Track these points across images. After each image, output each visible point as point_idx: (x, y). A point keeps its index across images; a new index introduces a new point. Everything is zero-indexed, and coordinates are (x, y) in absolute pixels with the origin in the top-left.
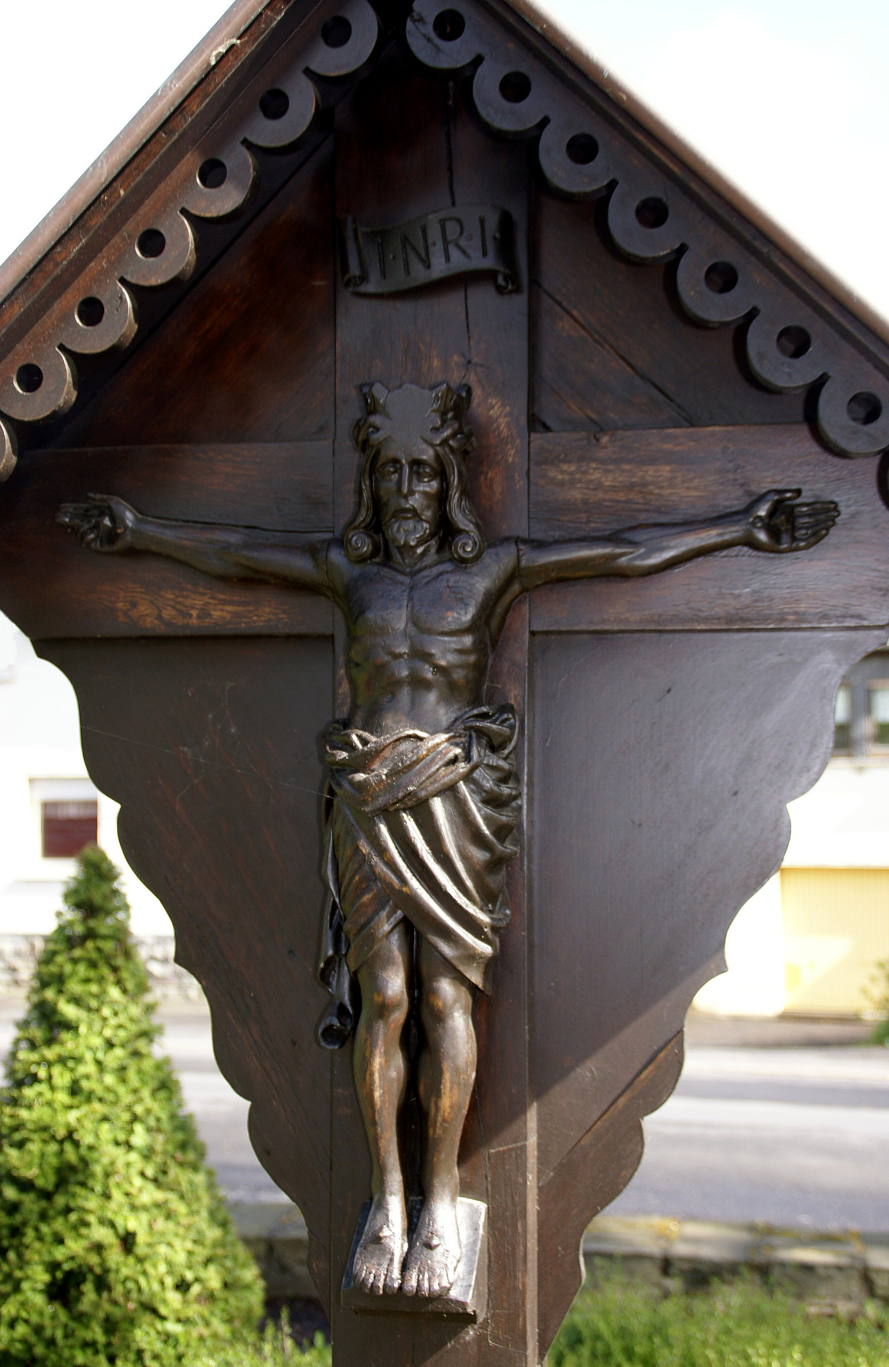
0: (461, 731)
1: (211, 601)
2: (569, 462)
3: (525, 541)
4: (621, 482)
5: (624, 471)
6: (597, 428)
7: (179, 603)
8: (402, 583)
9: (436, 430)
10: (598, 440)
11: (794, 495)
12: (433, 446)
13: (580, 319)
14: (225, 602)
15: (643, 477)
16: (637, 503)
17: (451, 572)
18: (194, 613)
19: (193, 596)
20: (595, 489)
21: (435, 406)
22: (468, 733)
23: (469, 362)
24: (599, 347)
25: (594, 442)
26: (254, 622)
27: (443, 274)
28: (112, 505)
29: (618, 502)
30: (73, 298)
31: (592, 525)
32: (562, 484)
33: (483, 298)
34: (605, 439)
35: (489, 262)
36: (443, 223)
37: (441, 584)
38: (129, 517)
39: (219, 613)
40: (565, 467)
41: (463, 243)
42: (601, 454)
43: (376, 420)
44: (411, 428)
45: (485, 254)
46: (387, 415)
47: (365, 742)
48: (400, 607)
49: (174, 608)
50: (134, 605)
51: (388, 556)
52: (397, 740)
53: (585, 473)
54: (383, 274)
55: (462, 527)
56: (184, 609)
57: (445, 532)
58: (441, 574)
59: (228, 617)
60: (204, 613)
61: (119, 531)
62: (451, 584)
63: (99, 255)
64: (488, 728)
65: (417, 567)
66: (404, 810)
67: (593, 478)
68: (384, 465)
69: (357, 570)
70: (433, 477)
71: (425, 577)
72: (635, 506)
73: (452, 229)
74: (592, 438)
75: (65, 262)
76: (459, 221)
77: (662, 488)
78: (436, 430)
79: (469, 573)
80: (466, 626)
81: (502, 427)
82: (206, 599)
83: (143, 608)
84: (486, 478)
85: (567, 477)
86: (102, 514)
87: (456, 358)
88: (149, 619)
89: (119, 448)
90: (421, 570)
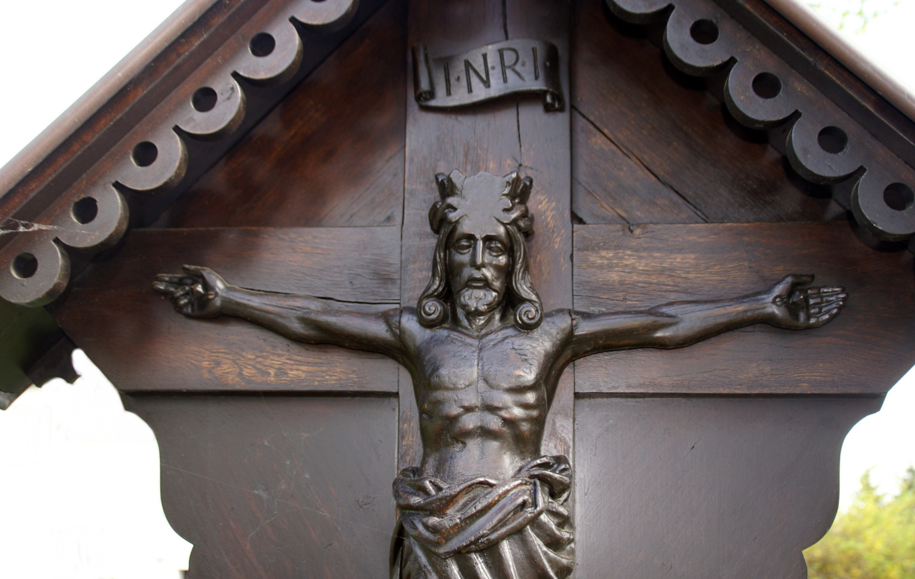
0: (527, 479)
1: (288, 362)
2: (607, 249)
3: (577, 313)
4: (652, 267)
5: (655, 258)
6: (629, 225)
7: (259, 362)
8: (471, 345)
9: (507, 210)
10: (632, 231)
11: (809, 279)
12: (504, 225)
13: (610, 136)
14: (300, 363)
15: (671, 263)
16: (667, 285)
17: (515, 336)
18: (272, 372)
19: (272, 357)
20: (630, 273)
21: (506, 192)
22: (532, 481)
23: (520, 165)
24: (626, 158)
25: (629, 233)
26: (327, 380)
27: (502, 93)
28: (205, 274)
29: (651, 283)
30: (190, 86)
31: (629, 302)
32: (601, 267)
33: (532, 115)
34: (638, 231)
35: (538, 85)
36: (501, 52)
37: (507, 346)
38: (220, 285)
39: (295, 372)
40: (603, 253)
41: (518, 68)
42: (634, 243)
43: (451, 200)
44: (481, 211)
45: (536, 78)
46: (462, 197)
47: (439, 489)
48: (471, 366)
49: (254, 367)
50: (218, 364)
51: (456, 322)
52: (470, 486)
53: (622, 258)
54: (449, 93)
55: (524, 295)
56: (264, 368)
57: (509, 301)
58: (507, 338)
59: (303, 375)
60: (281, 372)
61: (211, 297)
62: (516, 347)
63: (215, 53)
64: (550, 476)
65: (483, 332)
66: (475, 552)
67: (628, 263)
68: (460, 239)
69: (428, 333)
70: (501, 252)
71: (492, 340)
72: (665, 288)
73: (509, 58)
74: (627, 230)
75: (187, 54)
76: (514, 50)
77: (688, 272)
78: (507, 210)
79: (531, 338)
80: (532, 383)
81: (549, 219)
82: (283, 359)
83: (225, 367)
84: (535, 262)
85: (606, 262)
86: (195, 282)
87: (509, 162)
88: (231, 377)
89: (212, 229)
90: (487, 334)
